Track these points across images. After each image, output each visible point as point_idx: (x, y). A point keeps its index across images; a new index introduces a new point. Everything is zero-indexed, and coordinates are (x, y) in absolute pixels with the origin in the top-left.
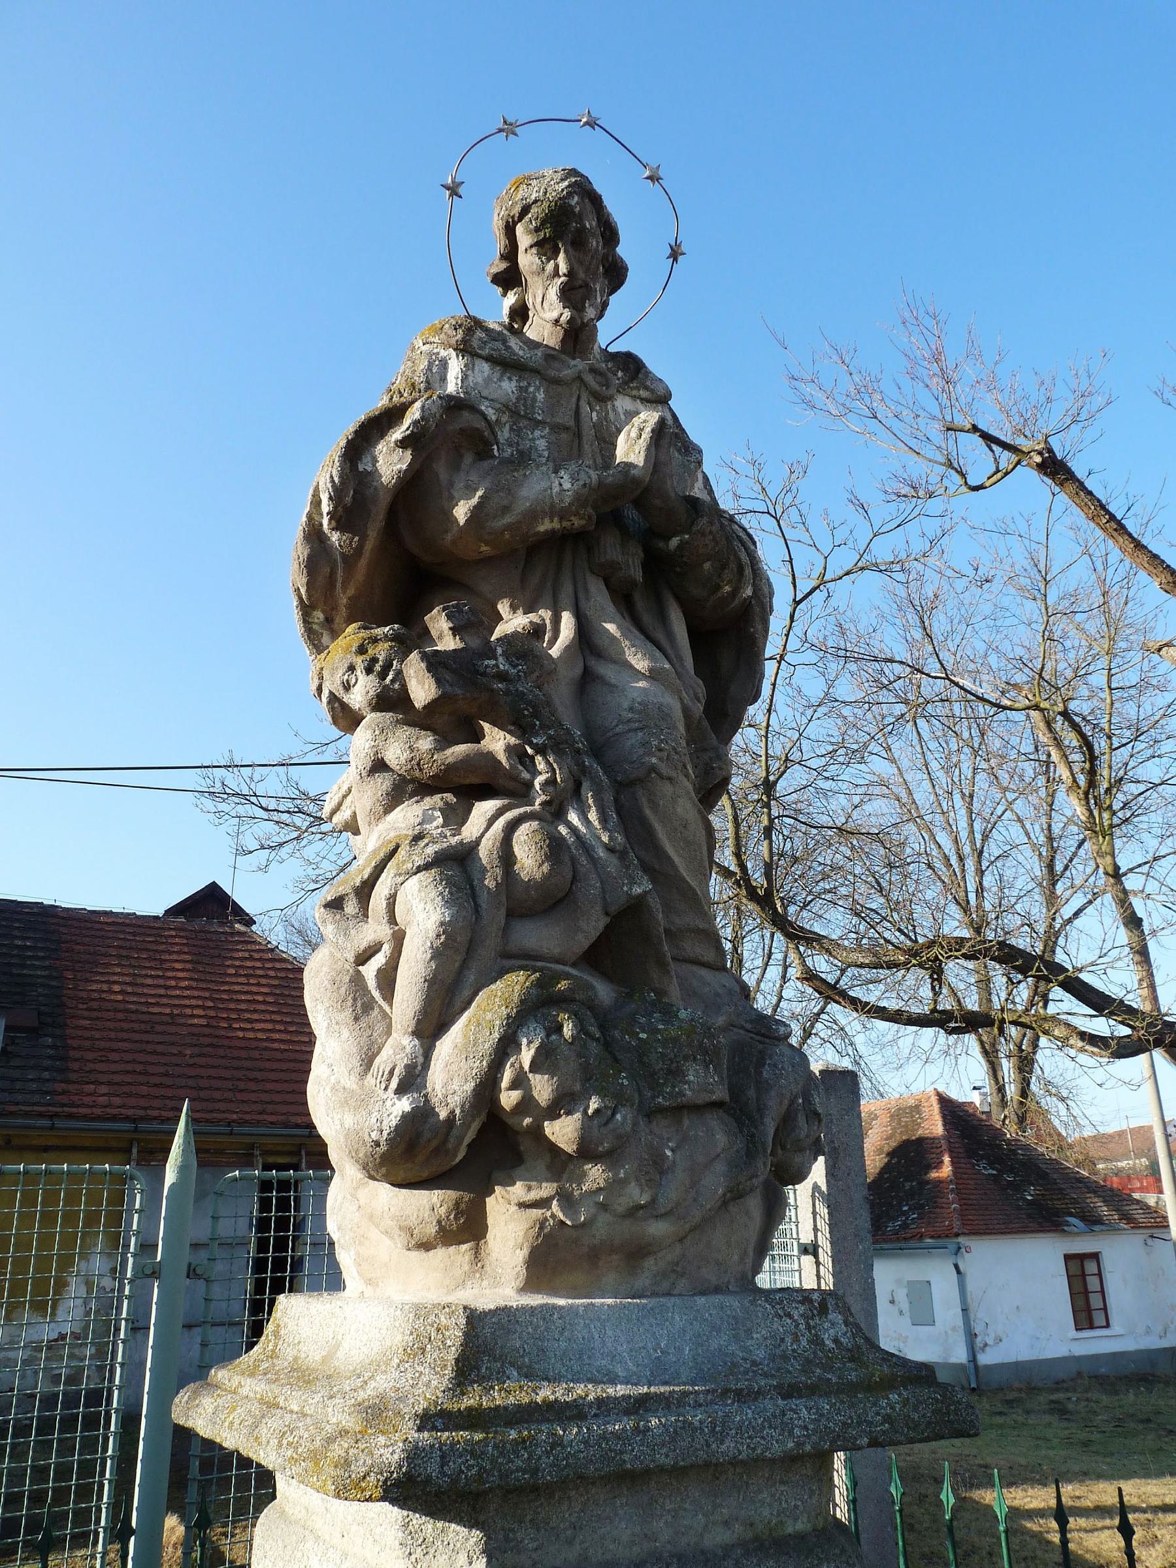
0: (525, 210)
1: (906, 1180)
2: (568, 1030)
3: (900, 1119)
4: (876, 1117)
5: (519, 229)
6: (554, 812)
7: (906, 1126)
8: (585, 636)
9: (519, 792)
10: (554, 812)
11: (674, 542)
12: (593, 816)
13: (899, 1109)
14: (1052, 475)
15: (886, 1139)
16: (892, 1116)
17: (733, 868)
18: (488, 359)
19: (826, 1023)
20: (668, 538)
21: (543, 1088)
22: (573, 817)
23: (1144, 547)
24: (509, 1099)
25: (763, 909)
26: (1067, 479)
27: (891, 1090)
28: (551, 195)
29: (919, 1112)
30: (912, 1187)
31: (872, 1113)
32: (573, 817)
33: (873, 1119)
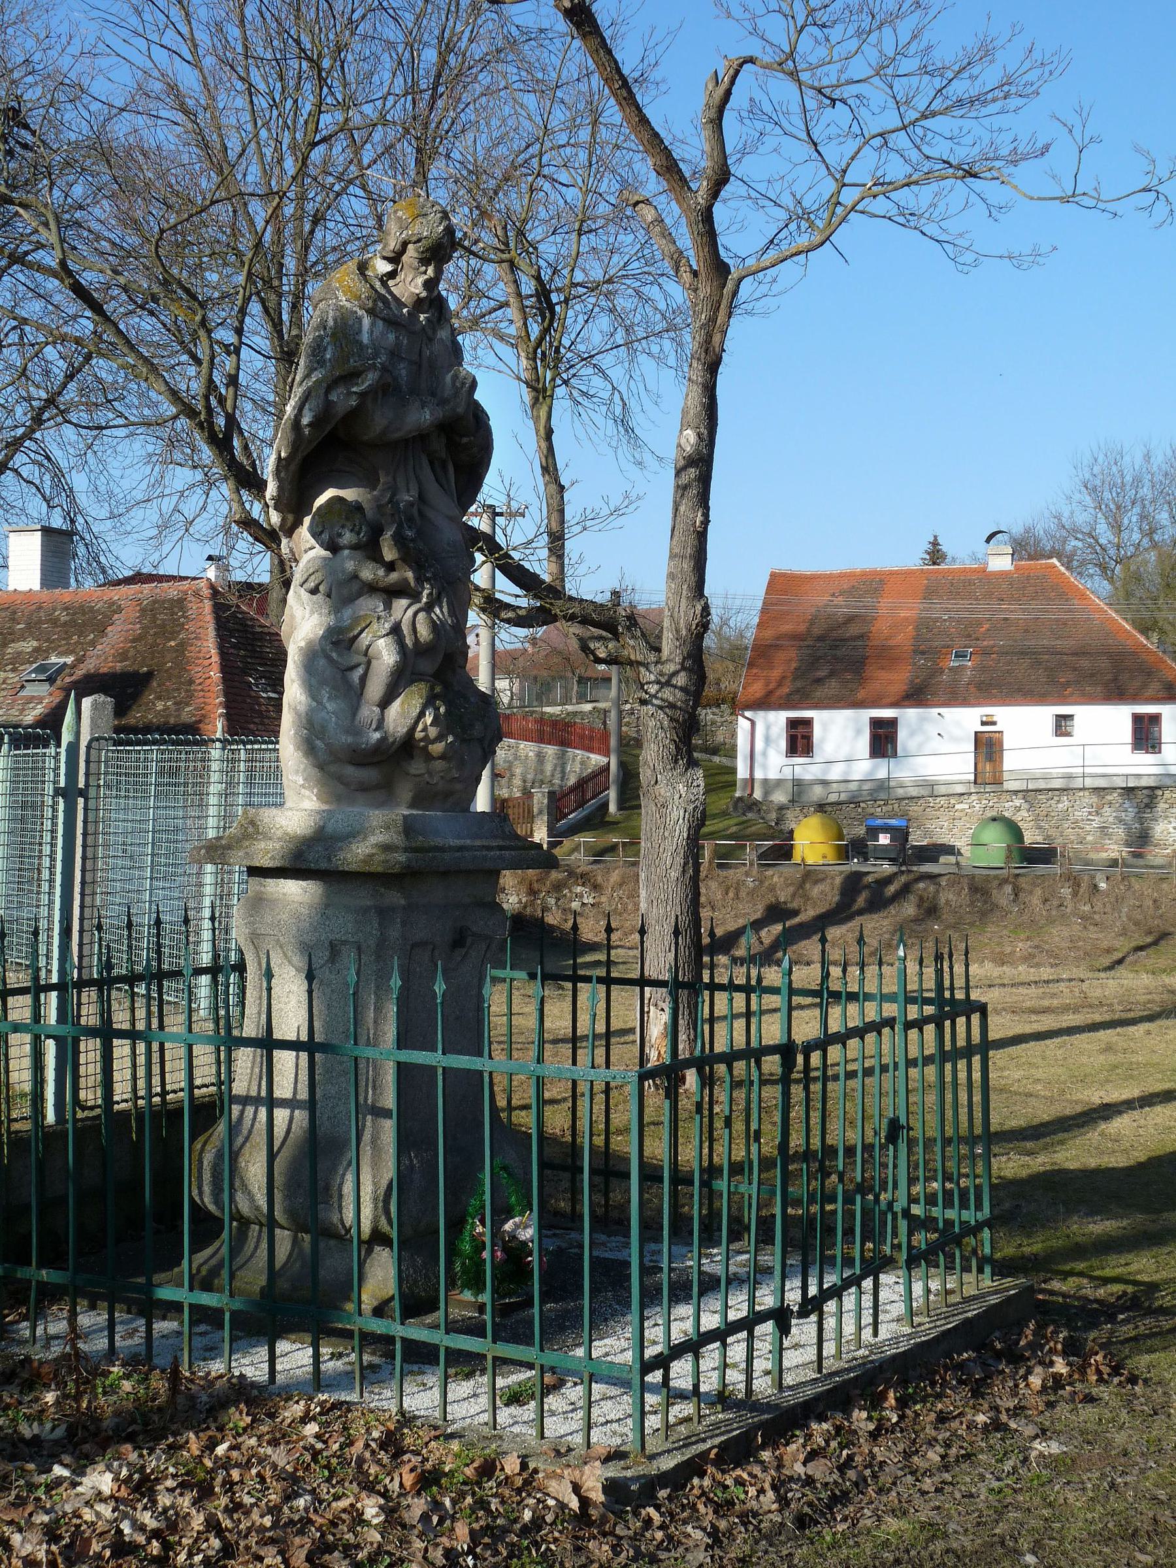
0: (419, 241)
1: (159, 698)
2: (442, 710)
3: (154, 616)
4: (119, 610)
5: (410, 246)
6: (428, 608)
7: (163, 626)
8: (422, 498)
9: (415, 597)
10: (428, 608)
11: (465, 440)
12: (445, 610)
13: (155, 602)
14: (578, 25)
15: (133, 641)
16: (143, 610)
17: (200, 407)
18: (384, 319)
19: (32, 455)
20: (462, 436)
21: (433, 732)
22: (437, 610)
23: (648, 122)
24: (419, 735)
25: (221, 453)
26: (590, 33)
27: (119, 564)
28: (434, 236)
29: (182, 609)
30: (166, 709)
31: (114, 603)
32: (437, 610)
33: (115, 612)
